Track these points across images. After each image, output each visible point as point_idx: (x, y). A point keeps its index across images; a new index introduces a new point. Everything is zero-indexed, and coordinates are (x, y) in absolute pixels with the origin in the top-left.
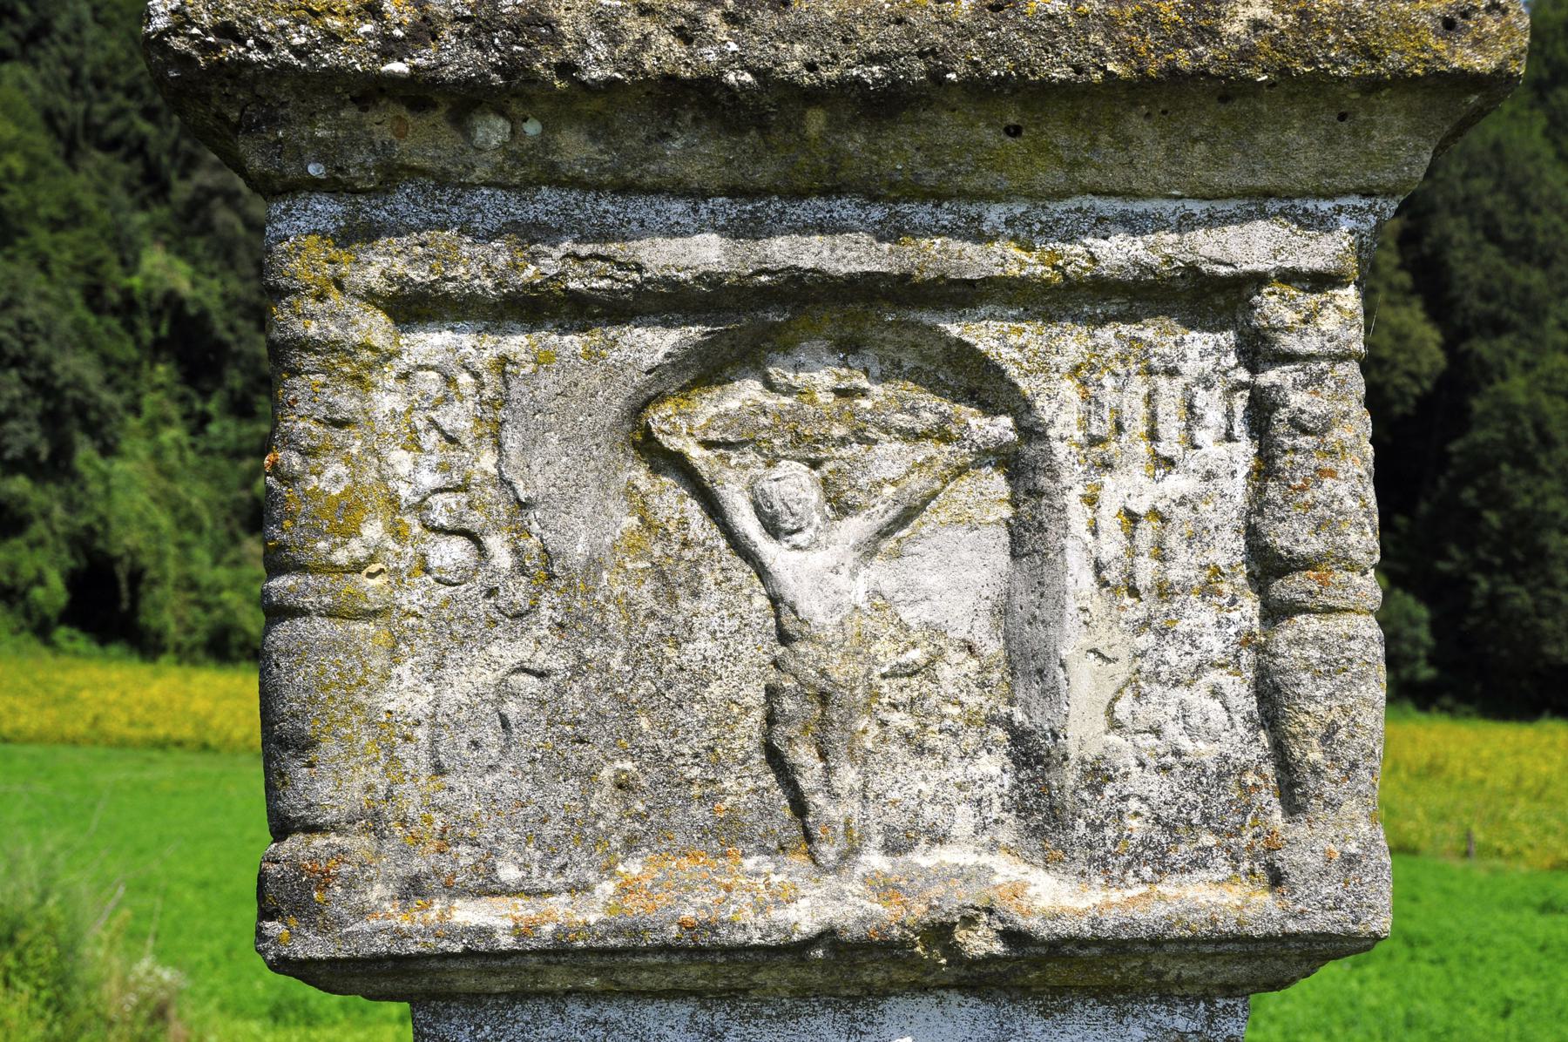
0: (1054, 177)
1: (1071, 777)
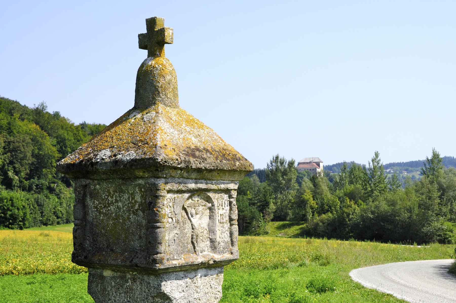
0: (219, 178)
1: (217, 244)
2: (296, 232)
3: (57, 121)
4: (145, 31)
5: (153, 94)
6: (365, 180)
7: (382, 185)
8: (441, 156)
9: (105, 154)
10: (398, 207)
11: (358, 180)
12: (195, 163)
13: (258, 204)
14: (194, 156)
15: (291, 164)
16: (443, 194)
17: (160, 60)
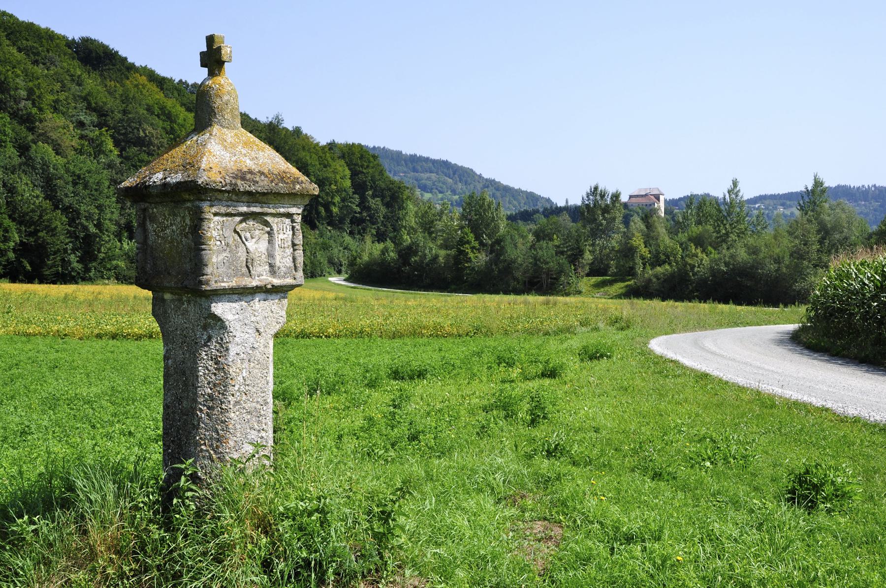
2: (621, 291)
3: (297, 141)
4: (205, 49)
5: (210, 115)
6: (718, 220)
7: (742, 226)
8: (826, 185)
9: (158, 177)
10: (762, 255)
11: (709, 216)
12: (242, 186)
13: (569, 253)
14: (243, 179)
15: (616, 197)
16: (824, 238)
17: (220, 80)
